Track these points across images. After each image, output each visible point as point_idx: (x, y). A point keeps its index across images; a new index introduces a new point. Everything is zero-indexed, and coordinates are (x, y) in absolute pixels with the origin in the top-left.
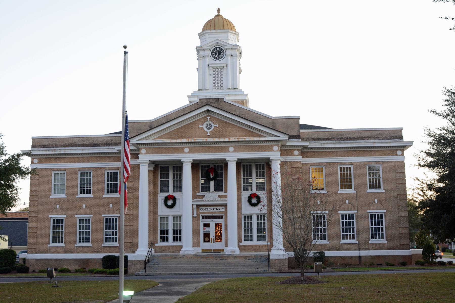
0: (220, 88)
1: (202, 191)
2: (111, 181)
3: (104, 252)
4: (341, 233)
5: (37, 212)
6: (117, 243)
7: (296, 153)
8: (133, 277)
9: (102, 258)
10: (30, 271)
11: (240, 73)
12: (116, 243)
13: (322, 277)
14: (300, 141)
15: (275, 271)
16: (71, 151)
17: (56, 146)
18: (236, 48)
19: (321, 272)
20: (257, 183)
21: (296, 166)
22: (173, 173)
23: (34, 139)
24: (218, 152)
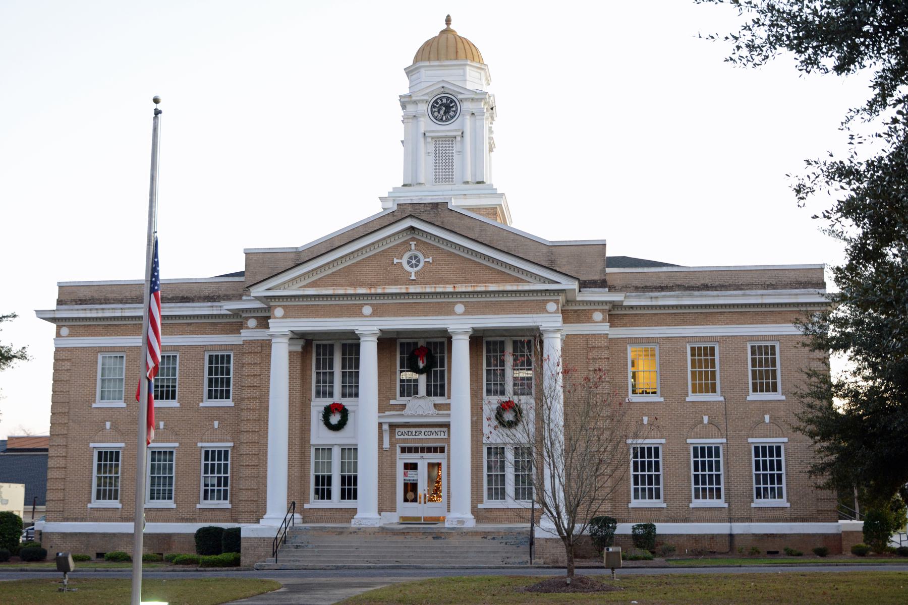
0: (449, 182)
1: (402, 395)
2: (216, 374)
3: (201, 521)
4: (693, 486)
5: (65, 436)
6: (228, 502)
7: (598, 316)
8: (251, 572)
9: (195, 532)
10: (48, 558)
11: (491, 150)
12: (225, 501)
13: (622, 578)
14: (605, 293)
15: (544, 564)
16: (135, 312)
17: (107, 301)
18: (480, 97)
19: (620, 568)
20: (515, 379)
21: (597, 344)
22: (342, 358)
23: (62, 287)
24: (432, 315)
